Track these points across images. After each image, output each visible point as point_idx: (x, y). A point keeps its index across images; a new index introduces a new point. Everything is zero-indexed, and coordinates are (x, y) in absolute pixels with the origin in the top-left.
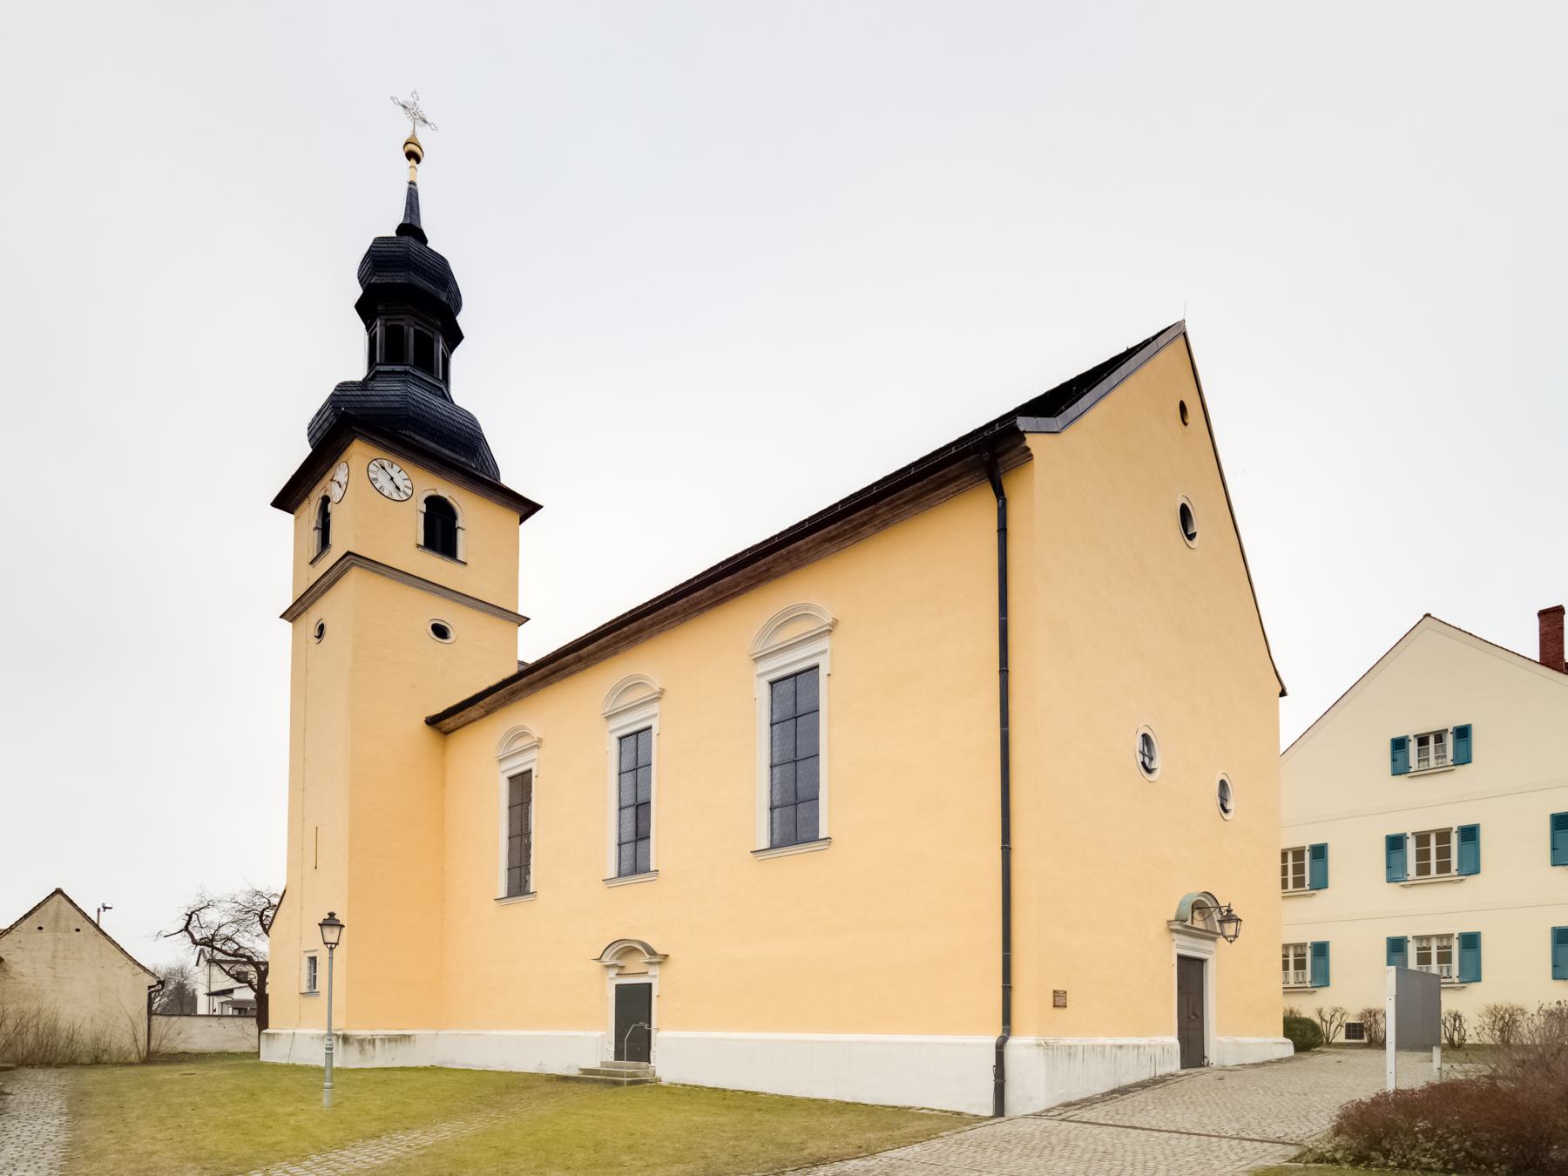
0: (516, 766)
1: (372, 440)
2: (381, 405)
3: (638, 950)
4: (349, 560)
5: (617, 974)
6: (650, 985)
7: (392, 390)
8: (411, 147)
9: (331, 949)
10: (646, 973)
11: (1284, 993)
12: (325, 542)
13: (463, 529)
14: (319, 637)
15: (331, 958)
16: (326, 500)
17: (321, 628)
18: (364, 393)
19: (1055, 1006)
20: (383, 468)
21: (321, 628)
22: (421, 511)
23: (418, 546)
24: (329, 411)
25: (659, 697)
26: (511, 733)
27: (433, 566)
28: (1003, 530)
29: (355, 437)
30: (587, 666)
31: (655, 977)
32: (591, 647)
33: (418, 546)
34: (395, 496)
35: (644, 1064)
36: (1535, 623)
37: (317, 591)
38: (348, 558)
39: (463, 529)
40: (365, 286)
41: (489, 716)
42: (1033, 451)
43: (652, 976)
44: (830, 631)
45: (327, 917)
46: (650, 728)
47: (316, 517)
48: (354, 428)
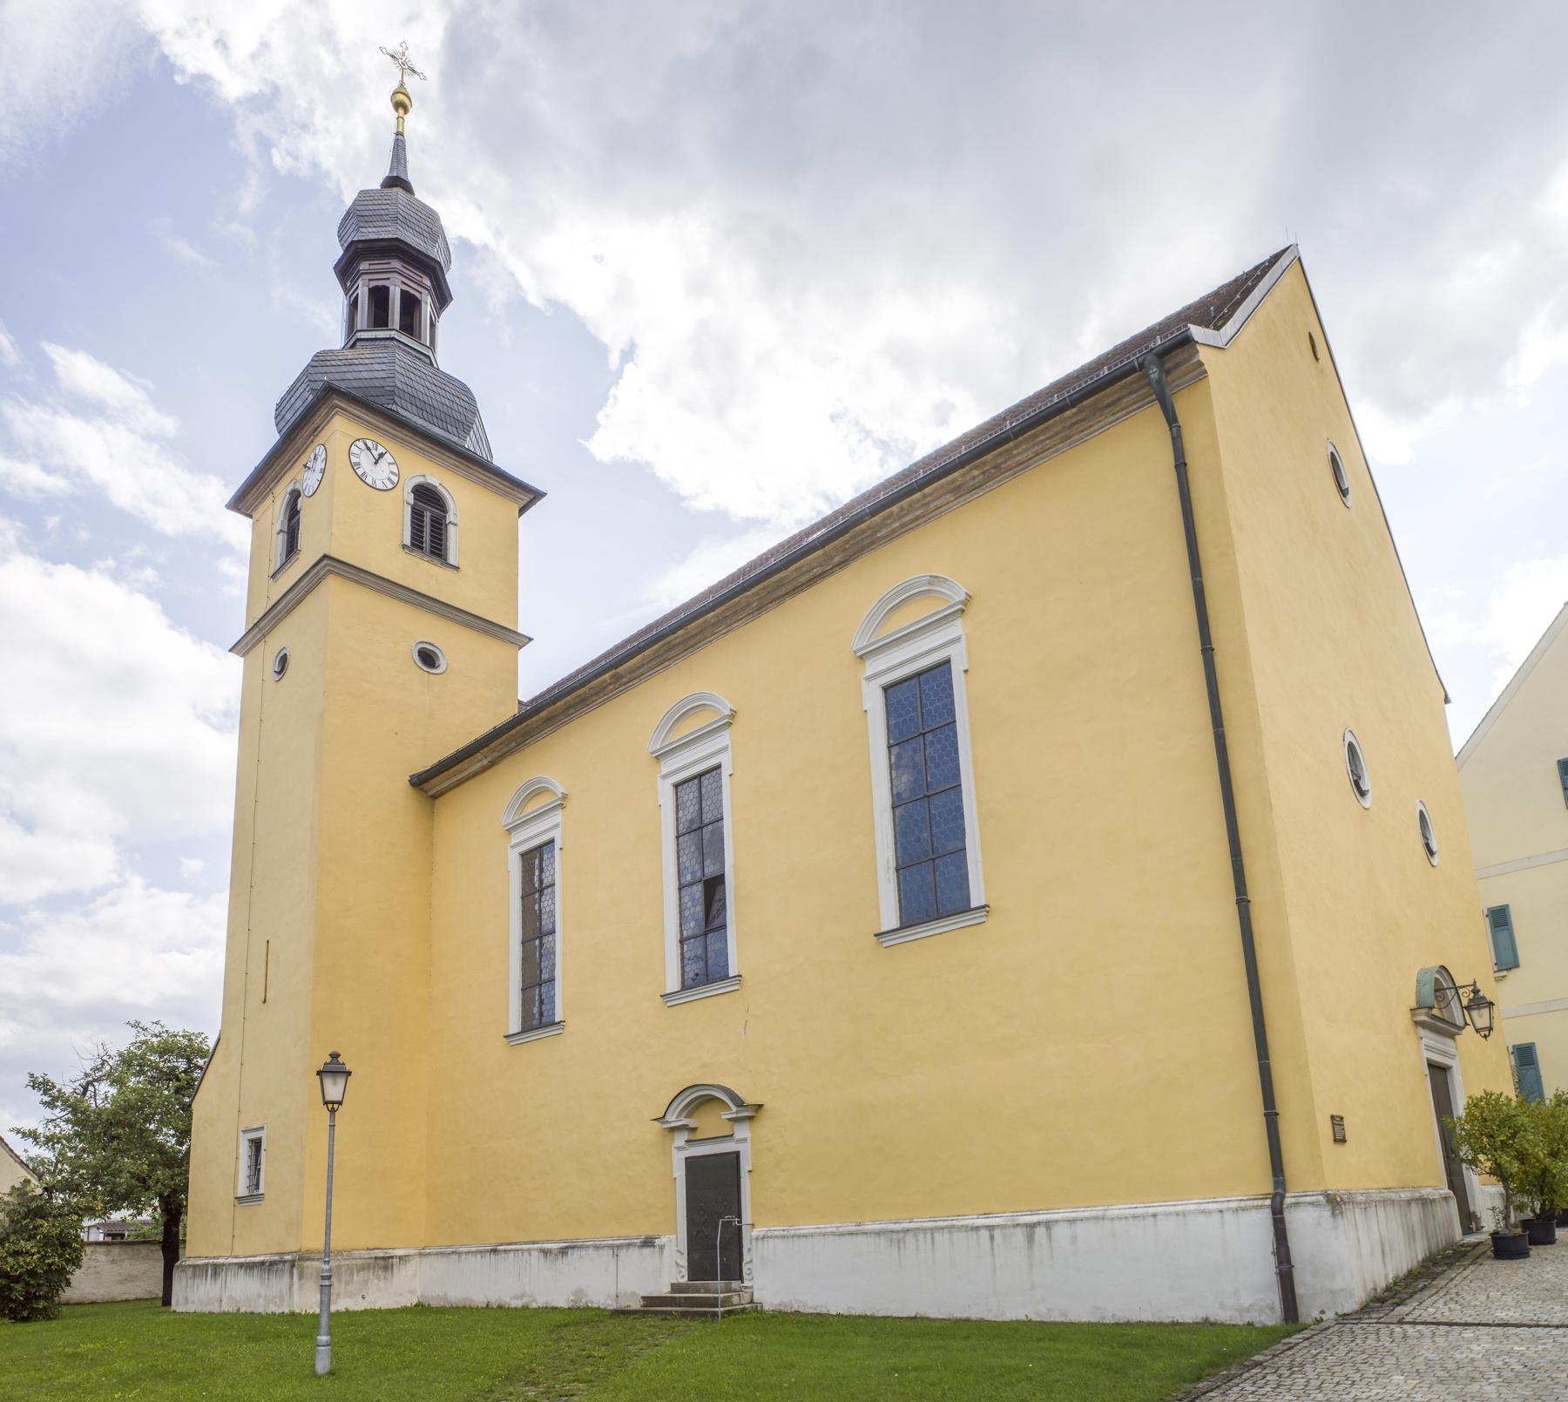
0: (531, 836)
2: (365, 375)
3: (718, 1098)
4: (326, 565)
5: (687, 1141)
6: (737, 1154)
7: (371, 367)
8: (401, 97)
9: (333, 1111)
10: (732, 1135)
12: (292, 547)
13: (455, 525)
14: (279, 673)
15: (332, 1126)
16: (295, 495)
17: (284, 661)
19: (1335, 1140)
20: (369, 449)
21: (284, 661)
22: (408, 503)
23: (404, 546)
24: (304, 386)
25: (729, 722)
26: (520, 795)
27: (419, 573)
28: (1181, 466)
31: (746, 1142)
33: (404, 546)
35: (735, 1284)
38: (325, 562)
39: (455, 525)
40: (346, 245)
41: (495, 768)
42: (1207, 367)
43: (739, 1141)
44: (963, 611)
45: (329, 1059)
46: (718, 767)
47: (281, 518)
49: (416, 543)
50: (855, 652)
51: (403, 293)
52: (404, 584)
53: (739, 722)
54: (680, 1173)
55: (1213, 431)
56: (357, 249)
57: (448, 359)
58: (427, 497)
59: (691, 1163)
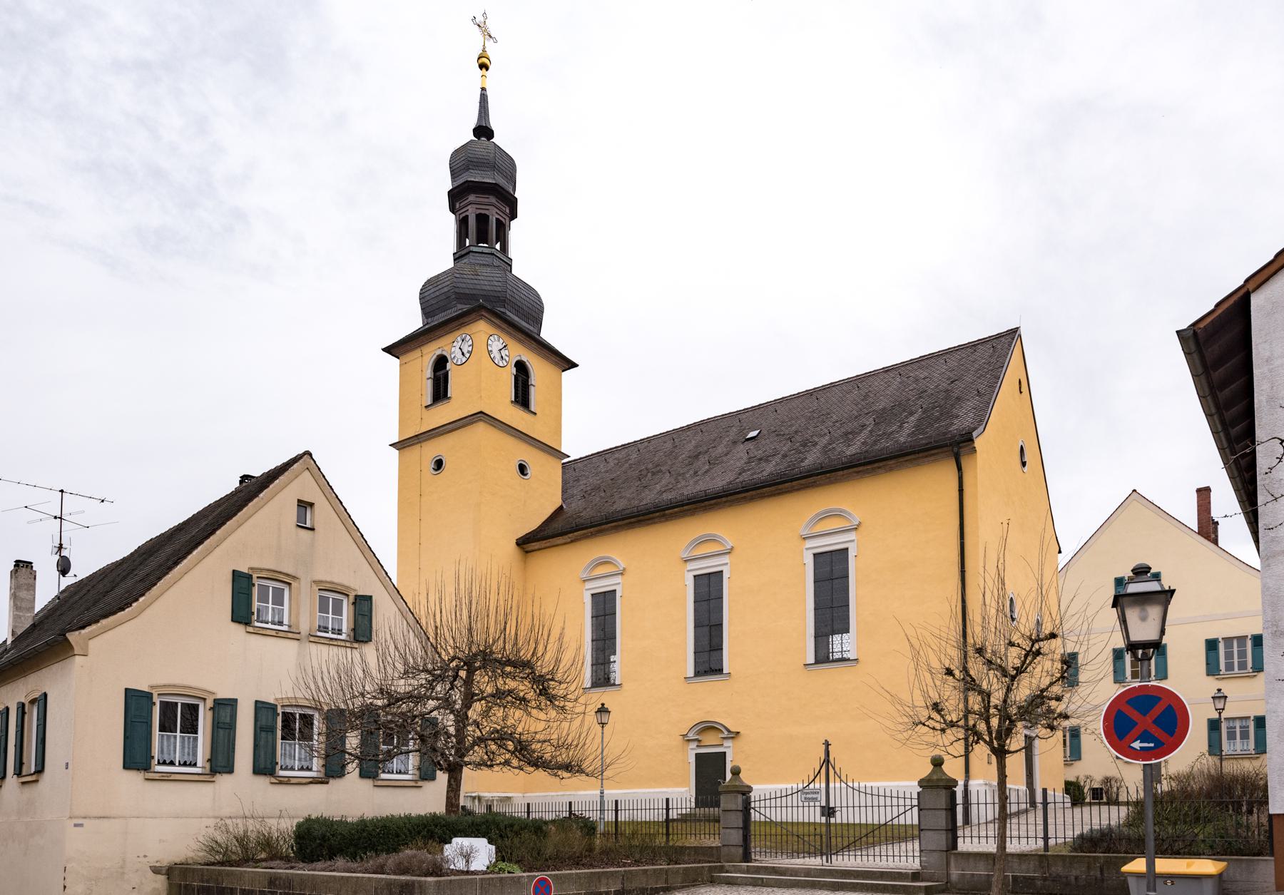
1: (492, 321)
2: (488, 288)
3: (717, 728)
6: (725, 753)
8: (484, 60)
11: (1065, 764)
13: (534, 386)
18: (476, 277)
28: (961, 491)
30: (667, 520)
32: (676, 509)
34: (501, 365)
36: (1195, 496)
37: (437, 433)
39: (534, 386)
42: (977, 449)
48: (483, 313)
50: (801, 536)
51: (497, 219)
52: (504, 421)
53: (734, 553)
54: (692, 760)
56: (469, 186)
57: (520, 269)
58: (521, 367)
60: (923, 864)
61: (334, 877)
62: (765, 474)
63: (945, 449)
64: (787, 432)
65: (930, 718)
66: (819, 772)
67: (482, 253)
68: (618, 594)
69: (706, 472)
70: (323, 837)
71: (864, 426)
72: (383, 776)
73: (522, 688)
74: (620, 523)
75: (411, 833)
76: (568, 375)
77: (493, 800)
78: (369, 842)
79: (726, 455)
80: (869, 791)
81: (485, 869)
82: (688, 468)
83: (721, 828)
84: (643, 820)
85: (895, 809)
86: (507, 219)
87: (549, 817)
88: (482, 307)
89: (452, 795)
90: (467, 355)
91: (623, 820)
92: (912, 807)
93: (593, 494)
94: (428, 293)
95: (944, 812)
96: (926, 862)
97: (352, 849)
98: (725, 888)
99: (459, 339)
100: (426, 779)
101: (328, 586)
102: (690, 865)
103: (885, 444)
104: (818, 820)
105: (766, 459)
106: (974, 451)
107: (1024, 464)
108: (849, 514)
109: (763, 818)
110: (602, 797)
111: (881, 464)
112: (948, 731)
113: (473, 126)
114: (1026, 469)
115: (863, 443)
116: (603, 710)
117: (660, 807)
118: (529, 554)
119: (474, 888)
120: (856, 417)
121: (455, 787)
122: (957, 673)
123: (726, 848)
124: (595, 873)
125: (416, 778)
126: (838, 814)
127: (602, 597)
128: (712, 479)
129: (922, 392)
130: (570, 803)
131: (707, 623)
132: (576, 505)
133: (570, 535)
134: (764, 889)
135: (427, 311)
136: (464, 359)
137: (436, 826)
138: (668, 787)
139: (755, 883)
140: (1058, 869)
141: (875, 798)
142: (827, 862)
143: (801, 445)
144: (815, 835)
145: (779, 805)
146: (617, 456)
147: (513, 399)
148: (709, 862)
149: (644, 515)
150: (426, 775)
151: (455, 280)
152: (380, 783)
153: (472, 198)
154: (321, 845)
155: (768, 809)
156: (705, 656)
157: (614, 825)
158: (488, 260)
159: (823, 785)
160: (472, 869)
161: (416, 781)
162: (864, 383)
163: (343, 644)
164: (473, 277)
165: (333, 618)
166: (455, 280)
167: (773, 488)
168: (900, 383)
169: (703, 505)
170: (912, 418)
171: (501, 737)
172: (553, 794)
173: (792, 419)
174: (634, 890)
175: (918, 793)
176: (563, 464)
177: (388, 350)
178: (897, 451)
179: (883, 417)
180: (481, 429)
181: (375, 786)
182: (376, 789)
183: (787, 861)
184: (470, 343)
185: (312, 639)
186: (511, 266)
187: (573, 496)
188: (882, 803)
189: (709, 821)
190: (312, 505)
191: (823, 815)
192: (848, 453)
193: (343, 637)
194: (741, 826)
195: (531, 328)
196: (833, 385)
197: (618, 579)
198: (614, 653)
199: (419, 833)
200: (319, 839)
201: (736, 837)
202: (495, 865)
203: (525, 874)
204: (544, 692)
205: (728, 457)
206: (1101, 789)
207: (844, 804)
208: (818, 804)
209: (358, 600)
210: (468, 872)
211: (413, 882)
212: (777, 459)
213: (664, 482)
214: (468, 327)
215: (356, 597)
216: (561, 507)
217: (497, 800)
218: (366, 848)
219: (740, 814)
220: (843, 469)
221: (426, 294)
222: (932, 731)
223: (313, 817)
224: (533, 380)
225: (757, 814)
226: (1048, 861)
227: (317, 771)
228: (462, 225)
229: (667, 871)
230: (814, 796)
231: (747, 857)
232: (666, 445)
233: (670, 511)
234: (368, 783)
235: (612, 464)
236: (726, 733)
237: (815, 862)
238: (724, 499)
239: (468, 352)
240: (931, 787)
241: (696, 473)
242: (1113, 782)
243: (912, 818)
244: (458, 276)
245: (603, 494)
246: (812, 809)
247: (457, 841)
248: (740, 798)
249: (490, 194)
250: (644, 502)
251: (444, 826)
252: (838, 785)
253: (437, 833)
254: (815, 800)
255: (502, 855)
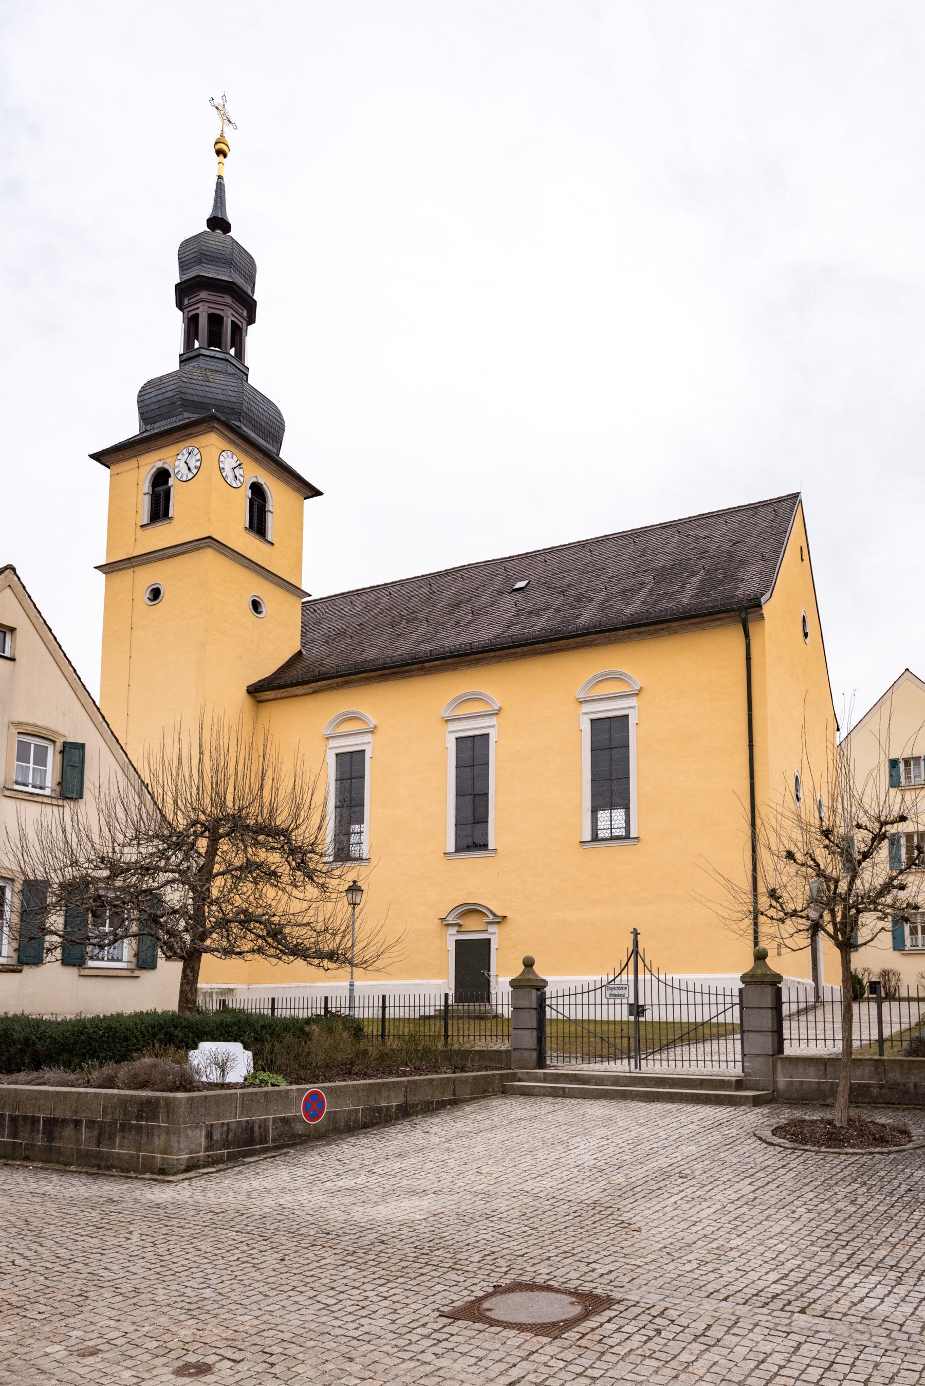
2: (222, 397)
6: (489, 940)
18: (207, 384)
27: (248, 545)
28: (748, 659)
29: (212, 431)
30: (426, 674)
31: (495, 935)
32: (437, 662)
34: (234, 485)
49: (251, 527)
51: (233, 322)
54: (452, 947)
55: (764, 645)
58: (257, 490)
59: (458, 942)
60: (746, 1070)
61: (46, 1092)
62: (537, 628)
63: (732, 614)
64: (558, 585)
65: (771, 906)
66: (627, 964)
67: (214, 357)
68: (368, 755)
69: (469, 623)
70: (27, 1041)
71: (643, 584)
72: (91, 963)
73: (271, 859)
74: (371, 674)
75: (143, 1036)
76: (310, 504)
77: (211, 994)
78: (89, 1047)
79: (491, 605)
80: (676, 985)
81: (241, 1080)
82: (449, 617)
83: (511, 1029)
84: (407, 1016)
85: (713, 1007)
86: (245, 323)
87: (304, 1014)
88: (213, 418)
89: (188, 988)
90: (195, 471)
91: (392, 1016)
92: (733, 1005)
93: (338, 639)
94: (149, 396)
95: (770, 1011)
96: (749, 1068)
97: (65, 1056)
98: (521, 1099)
99: (185, 451)
100: (145, 968)
101: (30, 729)
102: (479, 1073)
103: (666, 605)
104: (625, 1019)
105: (536, 613)
106: (762, 617)
107: (806, 635)
108: (630, 678)
109: (560, 1017)
110: (351, 990)
111: (664, 626)
112: (788, 921)
113: (208, 217)
114: (808, 640)
115: (643, 602)
116: (354, 888)
117: (376, 1005)
118: (261, 704)
119: (234, 1105)
120: (634, 574)
121: (191, 978)
122: (799, 856)
123: (517, 1053)
124: (374, 1084)
125: (133, 966)
126: (648, 1013)
127: (348, 757)
128: (477, 631)
129: (703, 553)
130: (273, 1000)
131: (470, 791)
132: (318, 651)
133: (312, 685)
134: (568, 1100)
135: (146, 416)
136: (190, 476)
137: (176, 1027)
138: (423, 978)
139: (556, 1094)
140: (895, 1076)
141: (691, 995)
142: (636, 1068)
143: (575, 600)
144: (622, 1037)
145: (579, 1002)
146: (364, 598)
147: (247, 526)
148: (497, 1069)
149: (399, 666)
150: (145, 963)
151: (182, 384)
152: (86, 972)
153: (204, 295)
154: (22, 1050)
155: (566, 1007)
156: (468, 829)
157: (380, 1023)
158: (221, 366)
159: (632, 977)
160: (227, 1081)
161: (132, 970)
162: (640, 538)
163: (46, 800)
164: (203, 383)
165: (34, 769)
166: (182, 384)
167: (547, 645)
168: (679, 541)
169: (467, 658)
170: (694, 579)
171: (246, 919)
172: (285, 985)
173: (563, 571)
174: (417, 1104)
175: (741, 990)
176: (303, 603)
177: (97, 457)
178: (681, 613)
179: (662, 575)
180: (209, 556)
181: (81, 976)
182: (82, 979)
183: (585, 1066)
184: (198, 457)
185: (7, 793)
186: (247, 375)
187: (313, 641)
188: (699, 1001)
189: (469, 1018)
190: (12, 630)
191: (631, 1014)
192: (628, 612)
193: (47, 792)
194: (535, 1026)
195: (270, 447)
196: (606, 538)
197: (368, 738)
198: (361, 821)
199: (154, 1036)
200: (21, 1044)
201: (529, 1039)
202: (254, 1077)
203: (294, 1087)
204: (302, 865)
205: (495, 607)
206: (879, 983)
207: (655, 1002)
208: (624, 1001)
209: (67, 749)
210: (223, 1086)
211: (158, 1099)
212: (549, 613)
213: (421, 631)
214: (196, 439)
215: (65, 744)
216: (300, 653)
217: (217, 993)
218: (84, 1055)
219: (534, 1013)
220: (624, 628)
221: (146, 397)
222: (769, 921)
223: (10, 1015)
224: (271, 505)
225: (554, 1013)
226: (884, 1067)
227: (8, 957)
228: (191, 324)
229: (455, 1080)
230: (621, 992)
231: (541, 1063)
232: (422, 590)
233: (431, 664)
234: (71, 973)
235: (360, 608)
236: (491, 917)
237: (621, 1067)
238: (492, 654)
239: (196, 467)
240: (755, 983)
241: (458, 623)
242: (891, 975)
243: (733, 1016)
244: (185, 380)
245: (349, 641)
246: (618, 1007)
247: (207, 1047)
248: (534, 994)
249: (199, 291)
250: (399, 652)
251: (185, 1027)
252: (648, 976)
253: (177, 1036)
254: (621, 996)
255: (262, 1062)
